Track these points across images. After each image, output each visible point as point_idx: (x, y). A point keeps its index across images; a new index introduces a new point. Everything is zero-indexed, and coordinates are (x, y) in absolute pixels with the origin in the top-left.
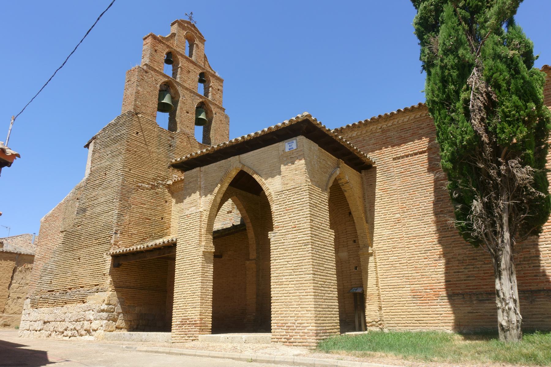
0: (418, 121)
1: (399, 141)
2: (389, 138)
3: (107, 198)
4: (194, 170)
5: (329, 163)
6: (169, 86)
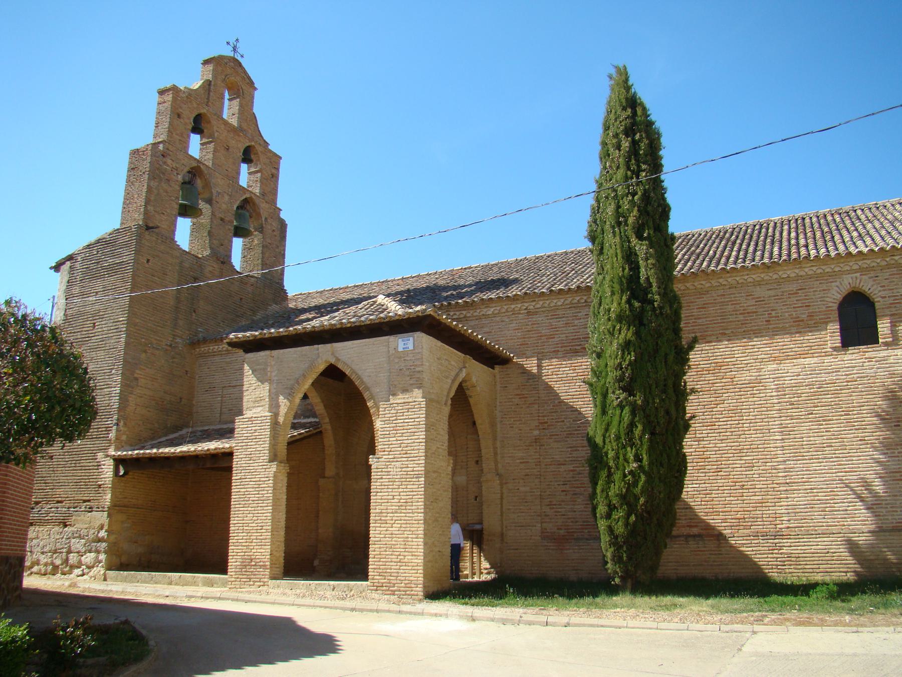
0: (574, 307)
1: (548, 331)
2: (535, 324)
3: (98, 366)
4: (262, 353)
5: (453, 363)
6: (195, 175)
